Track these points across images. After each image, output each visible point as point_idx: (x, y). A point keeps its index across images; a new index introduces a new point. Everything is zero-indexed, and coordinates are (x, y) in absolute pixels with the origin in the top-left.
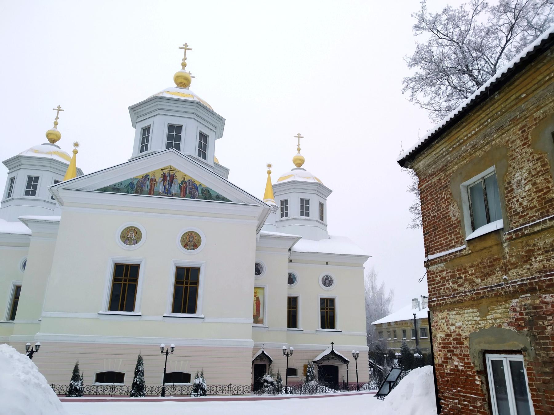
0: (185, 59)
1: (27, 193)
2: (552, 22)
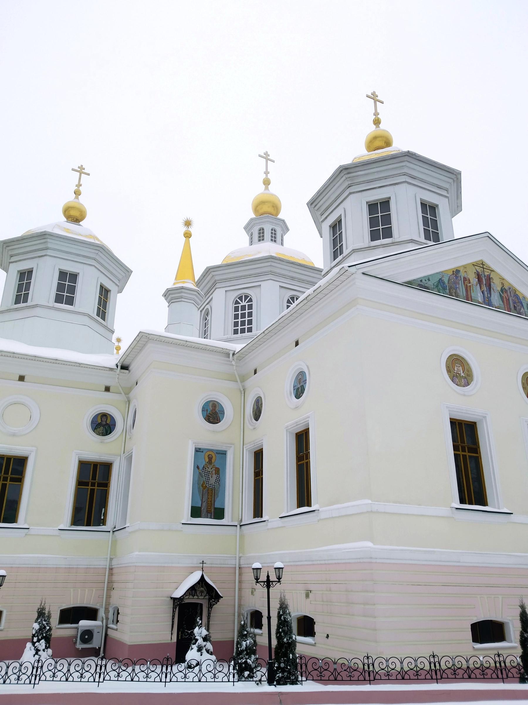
0: (79, 185)
1: (374, 236)
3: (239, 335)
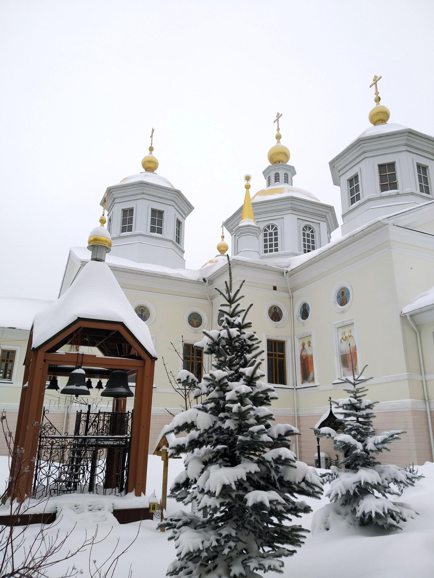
0: (377, 93)
3: (269, 253)
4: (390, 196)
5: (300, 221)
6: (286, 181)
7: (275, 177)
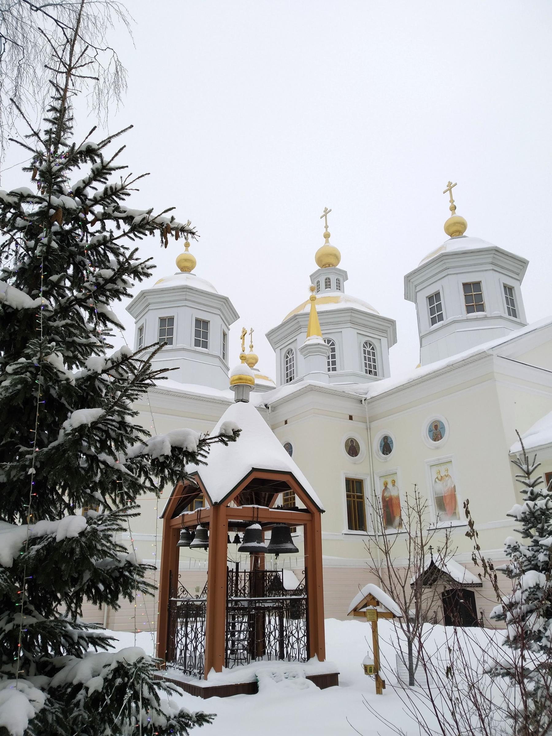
0: (452, 201)
2: (532, 700)
4: (477, 319)
5: (359, 335)
6: (339, 287)
7: (326, 282)
